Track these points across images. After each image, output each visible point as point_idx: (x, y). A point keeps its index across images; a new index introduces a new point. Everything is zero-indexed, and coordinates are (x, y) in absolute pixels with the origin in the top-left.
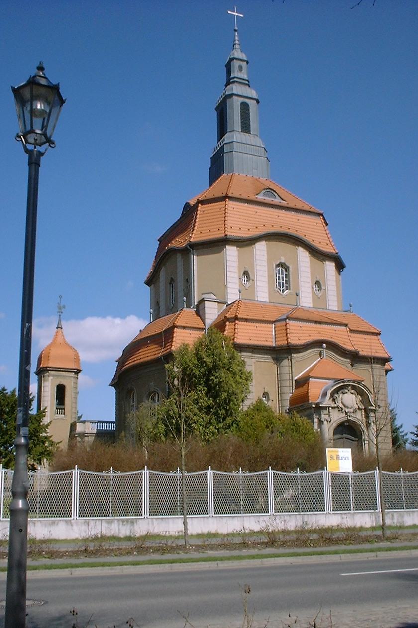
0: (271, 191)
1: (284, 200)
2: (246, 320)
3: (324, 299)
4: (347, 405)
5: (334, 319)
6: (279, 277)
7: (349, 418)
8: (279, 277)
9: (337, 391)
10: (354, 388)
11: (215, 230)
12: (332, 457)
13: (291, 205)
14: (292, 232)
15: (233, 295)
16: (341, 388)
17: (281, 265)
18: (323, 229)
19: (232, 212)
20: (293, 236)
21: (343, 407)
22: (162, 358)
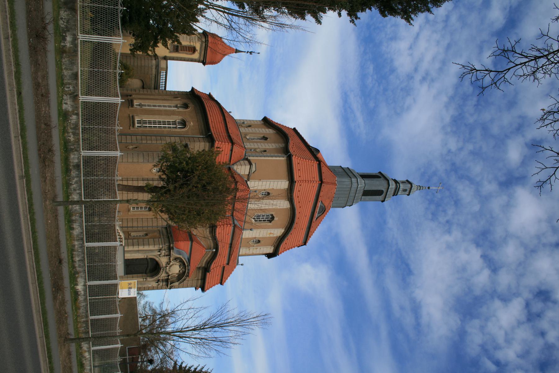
1: (316, 219)
2: (232, 150)
3: (248, 246)
4: (172, 268)
6: (264, 216)
7: (162, 269)
8: (264, 216)
9: (181, 261)
10: (184, 273)
11: (299, 167)
12: (130, 284)
14: (295, 225)
15: (253, 184)
16: (184, 264)
17: (273, 218)
20: (292, 226)
21: (170, 265)
22: (210, 133)
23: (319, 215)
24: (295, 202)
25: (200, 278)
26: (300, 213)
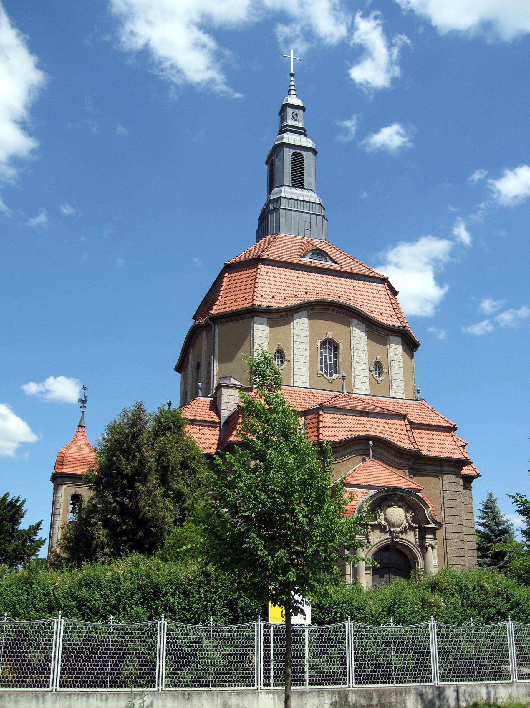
0: (319, 253)
5: (389, 409)
13: (346, 269)
18: (388, 297)
19: (265, 277)
23: (328, 260)
24: (295, 302)
25: (439, 468)
26: (318, 294)
